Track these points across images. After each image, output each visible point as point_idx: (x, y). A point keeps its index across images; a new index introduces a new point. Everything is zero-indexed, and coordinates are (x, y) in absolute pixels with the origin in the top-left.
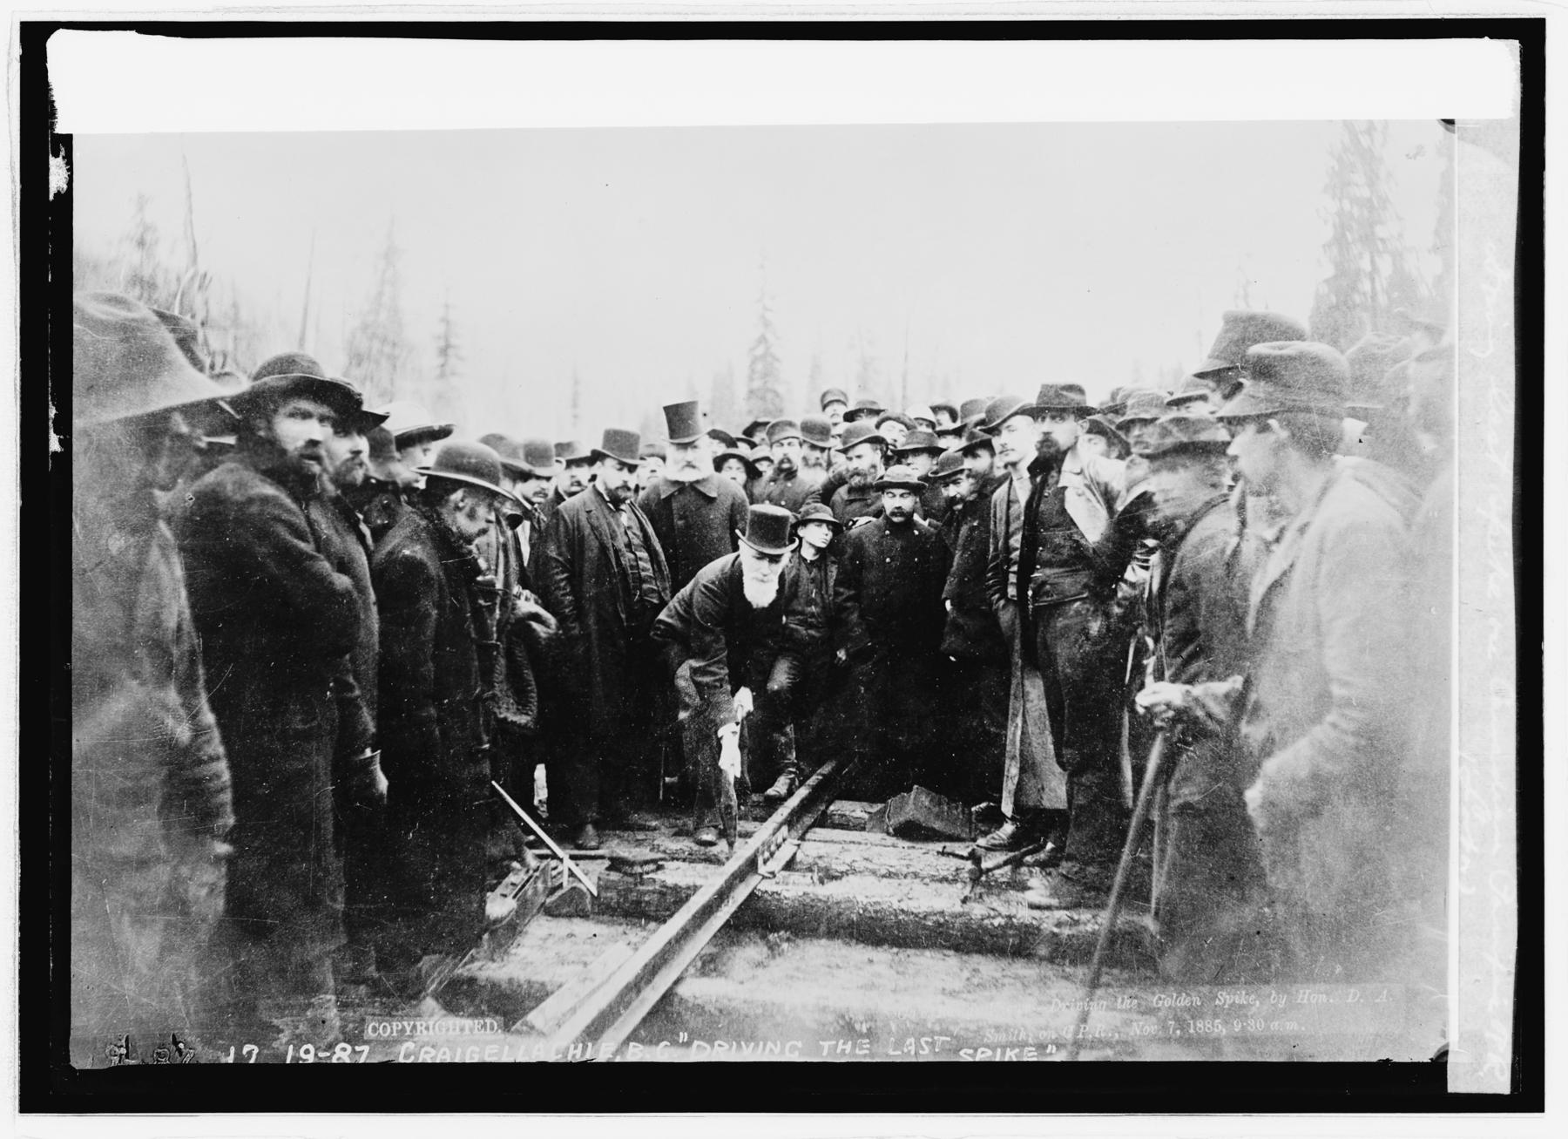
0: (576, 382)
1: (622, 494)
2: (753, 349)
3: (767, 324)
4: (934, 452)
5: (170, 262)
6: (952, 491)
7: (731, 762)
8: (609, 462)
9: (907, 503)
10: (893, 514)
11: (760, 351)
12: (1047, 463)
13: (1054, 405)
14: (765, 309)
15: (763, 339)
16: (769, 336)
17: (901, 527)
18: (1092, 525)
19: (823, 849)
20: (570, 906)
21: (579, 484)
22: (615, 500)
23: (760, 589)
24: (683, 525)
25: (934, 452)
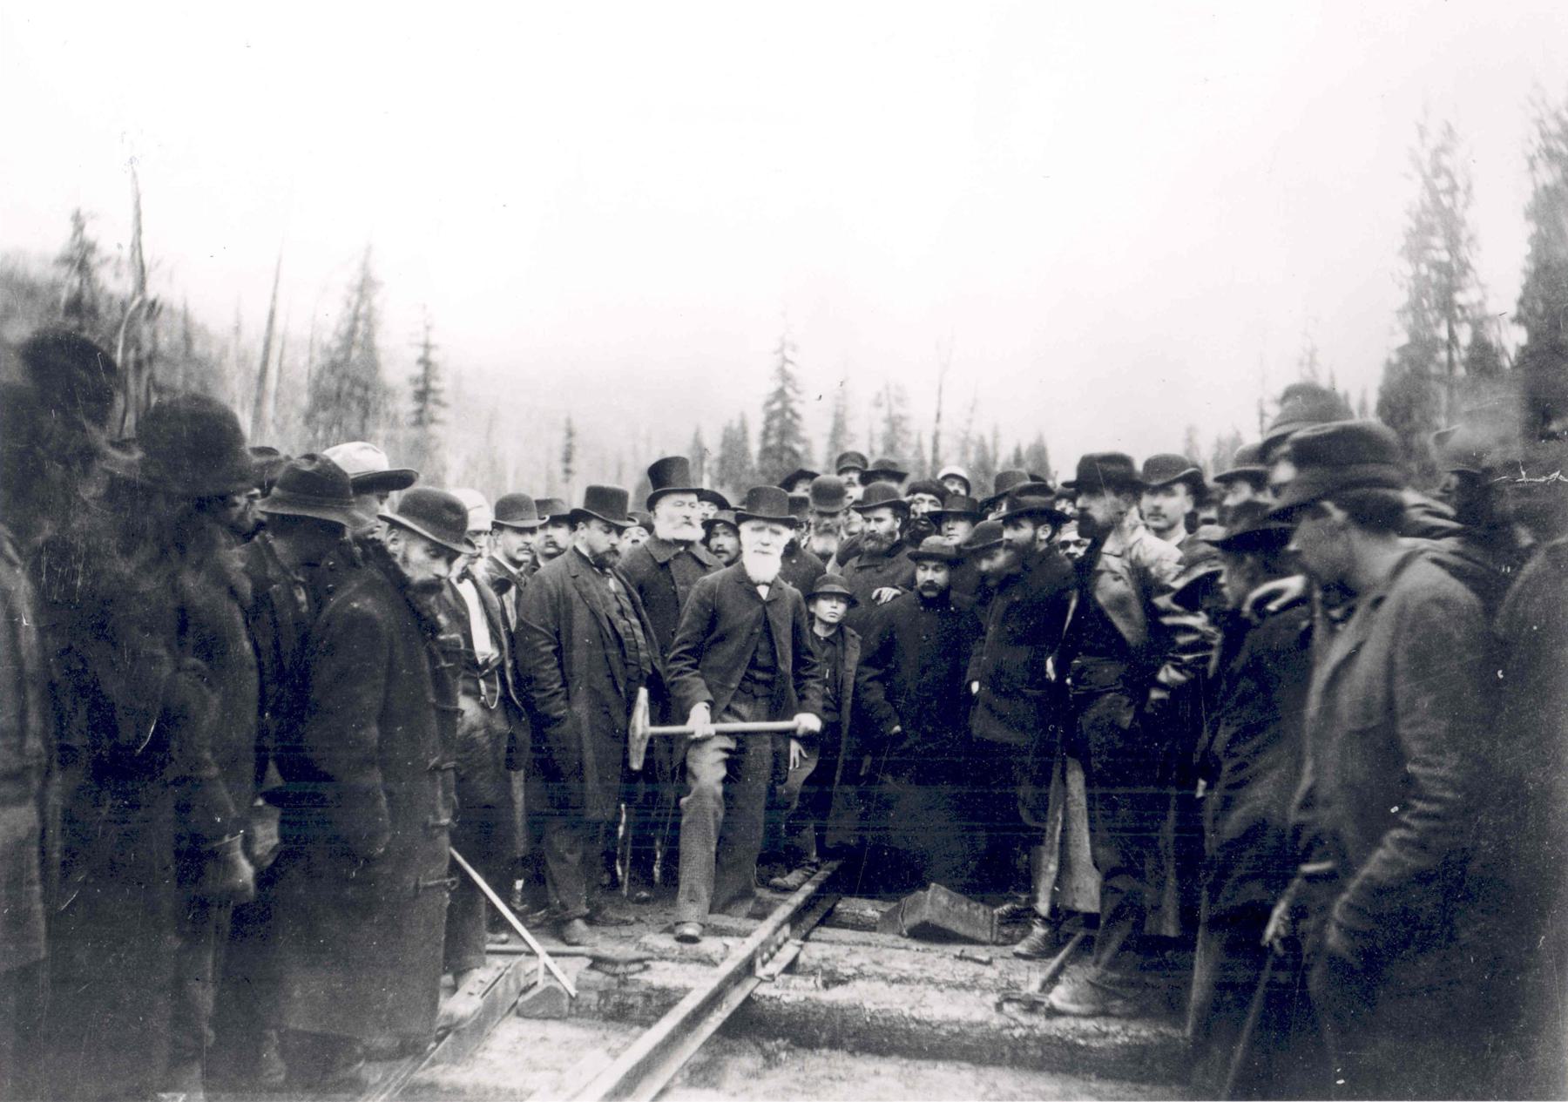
0: (570, 434)
2: (769, 404)
3: (786, 377)
8: (594, 524)
9: (940, 577)
10: (924, 588)
11: (777, 406)
14: (785, 360)
15: (780, 394)
16: (789, 391)
17: (937, 600)
19: (829, 951)
21: (554, 544)
22: (599, 563)
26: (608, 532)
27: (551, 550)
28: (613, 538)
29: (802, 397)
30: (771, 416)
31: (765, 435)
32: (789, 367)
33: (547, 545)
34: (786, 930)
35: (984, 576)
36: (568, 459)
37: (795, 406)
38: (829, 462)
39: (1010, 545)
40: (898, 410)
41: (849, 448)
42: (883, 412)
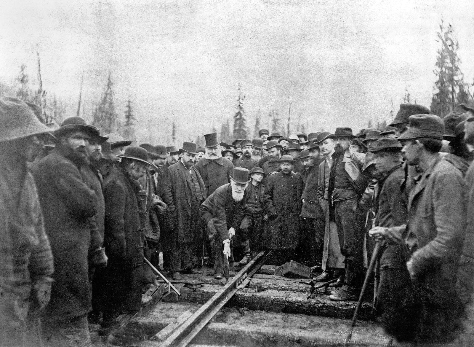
0: (174, 127)
1: (190, 164)
3: (241, 108)
4: (298, 150)
5: (266, 125)
6: (305, 163)
7: (227, 251)
10: (284, 171)
11: (238, 117)
12: (339, 154)
13: (343, 134)
14: (240, 103)
16: (242, 112)
18: (354, 175)
19: (259, 281)
20: (170, 298)
22: (187, 166)
23: (238, 195)
24: (209, 172)
25: (298, 150)
26: (189, 156)
27: (173, 162)
28: (191, 158)
29: (246, 114)
30: (236, 120)
31: (235, 126)
32: (241, 105)
33: (173, 161)
34: (246, 274)
35: (305, 166)
36: (174, 135)
37: (244, 117)
38: (256, 134)
39: (312, 158)
40: (276, 117)
41: (261, 129)
42: (272, 118)
